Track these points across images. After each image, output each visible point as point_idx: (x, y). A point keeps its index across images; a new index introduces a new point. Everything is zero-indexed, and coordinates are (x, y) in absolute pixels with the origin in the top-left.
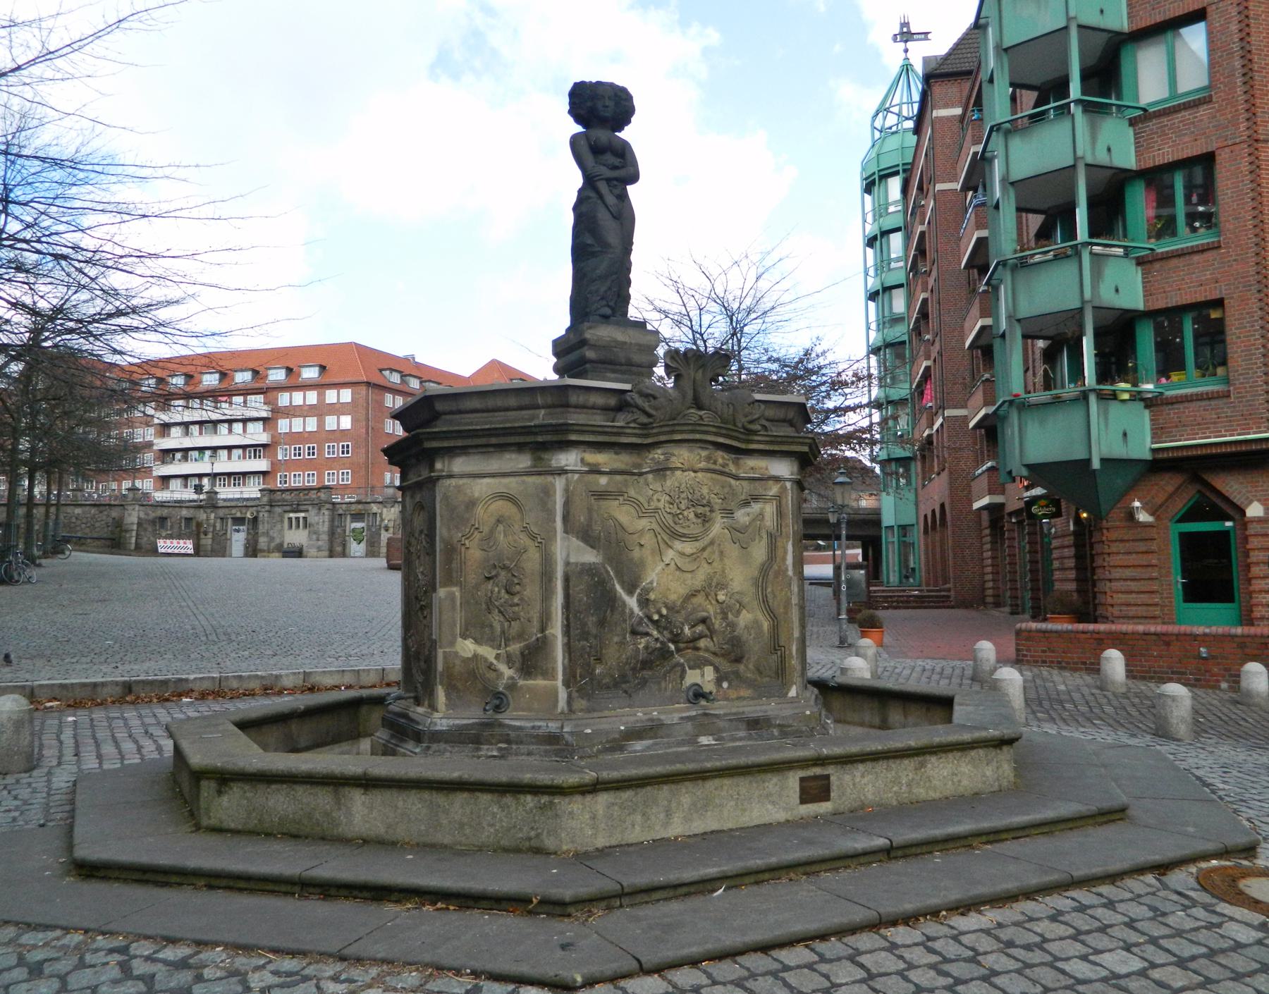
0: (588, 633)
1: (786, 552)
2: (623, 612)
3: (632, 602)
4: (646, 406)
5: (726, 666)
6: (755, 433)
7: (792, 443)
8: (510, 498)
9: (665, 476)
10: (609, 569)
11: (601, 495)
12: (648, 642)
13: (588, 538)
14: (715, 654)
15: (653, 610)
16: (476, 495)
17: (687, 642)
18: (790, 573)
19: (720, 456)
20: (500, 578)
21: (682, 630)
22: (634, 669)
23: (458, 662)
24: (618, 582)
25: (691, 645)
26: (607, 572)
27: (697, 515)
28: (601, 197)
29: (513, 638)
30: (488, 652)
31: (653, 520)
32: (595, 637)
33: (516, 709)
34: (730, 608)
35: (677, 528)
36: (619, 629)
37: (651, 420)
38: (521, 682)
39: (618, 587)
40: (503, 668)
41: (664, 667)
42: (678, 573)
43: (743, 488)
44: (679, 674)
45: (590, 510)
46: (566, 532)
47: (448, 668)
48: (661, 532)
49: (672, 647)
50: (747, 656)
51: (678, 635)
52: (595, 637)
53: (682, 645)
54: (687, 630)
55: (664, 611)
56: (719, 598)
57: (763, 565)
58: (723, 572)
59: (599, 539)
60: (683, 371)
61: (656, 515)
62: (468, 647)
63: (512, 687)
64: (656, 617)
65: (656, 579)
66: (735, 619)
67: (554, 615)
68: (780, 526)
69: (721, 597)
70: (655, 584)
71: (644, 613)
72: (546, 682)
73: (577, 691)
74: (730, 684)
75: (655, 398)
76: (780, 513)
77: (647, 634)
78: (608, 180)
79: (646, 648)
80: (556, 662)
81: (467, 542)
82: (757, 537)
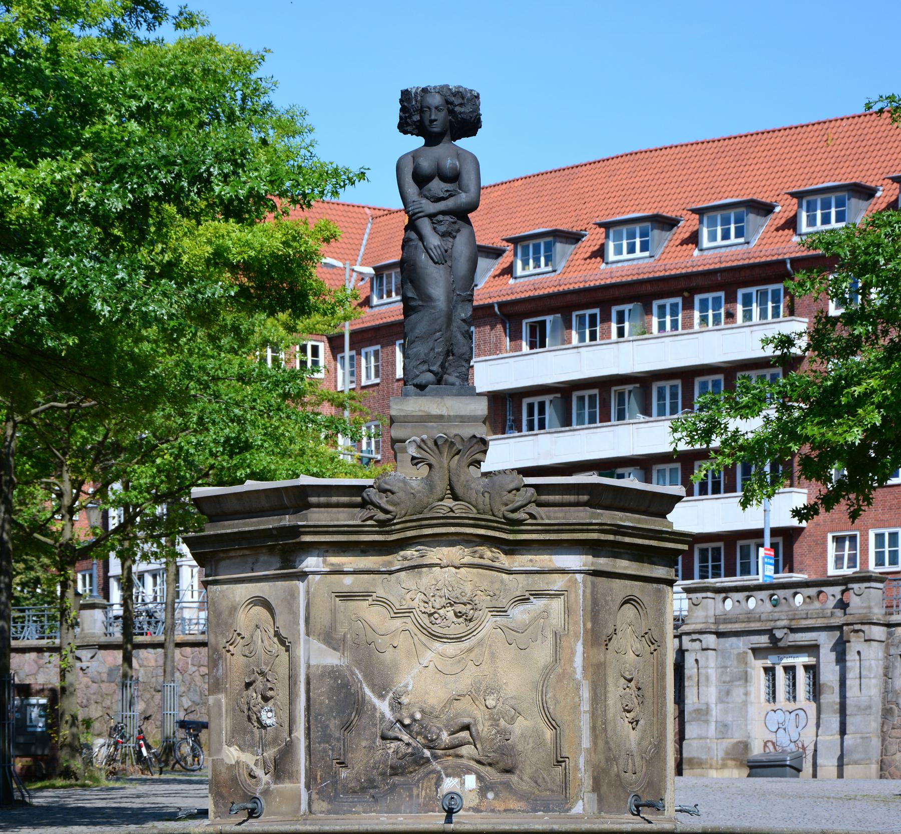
0: (330, 736)
1: (573, 653)
2: (373, 716)
3: (384, 707)
4: (383, 502)
5: (492, 774)
6: (520, 522)
7: (588, 531)
8: (265, 603)
9: (420, 573)
10: (357, 672)
11: (347, 597)
12: (399, 747)
13: (330, 639)
14: (479, 762)
15: (405, 714)
16: (238, 599)
17: (445, 749)
18: (579, 675)
19: (487, 554)
20: (257, 683)
21: (438, 735)
22: (383, 774)
23: (224, 770)
24: (368, 685)
25: (451, 751)
26: (353, 673)
27: (458, 615)
28: (421, 238)
29: (270, 743)
30: (248, 758)
31: (408, 620)
32: (338, 740)
33: (269, 814)
34: (502, 715)
35: (435, 628)
36: (367, 732)
37: (389, 516)
38: (273, 786)
39: (368, 691)
40: (259, 772)
41: (419, 773)
42: (438, 676)
43: (518, 585)
44: (434, 780)
45: (334, 612)
46: (308, 634)
47: (216, 775)
48: (418, 632)
49: (427, 753)
50: (520, 767)
51: (432, 741)
52: (338, 740)
53: (440, 752)
54: (445, 736)
55: (418, 716)
56: (487, 703)
57: (546, 667)
58: (495, 675)
59: (344, 639)
60: (432, 460)
61: (411, 615)
62: (232, 754)
63: (266, 792)
64: (407, 721)
65: (411, 682)
66: (508, 726)
67: (298, 719)
68: (566, 622)
69: (491, 702)
70: (410, 688)
71: (395, 718)
72: (292, 785)
73: (317, 793)
74: (496, 795)
75: (393, 493)
76: (568, 611)
77: (397, 739)
78: (431, 216)
79: (396, 752)
80: (299, 764)
81: (231, 648)
82: (540, 637)
